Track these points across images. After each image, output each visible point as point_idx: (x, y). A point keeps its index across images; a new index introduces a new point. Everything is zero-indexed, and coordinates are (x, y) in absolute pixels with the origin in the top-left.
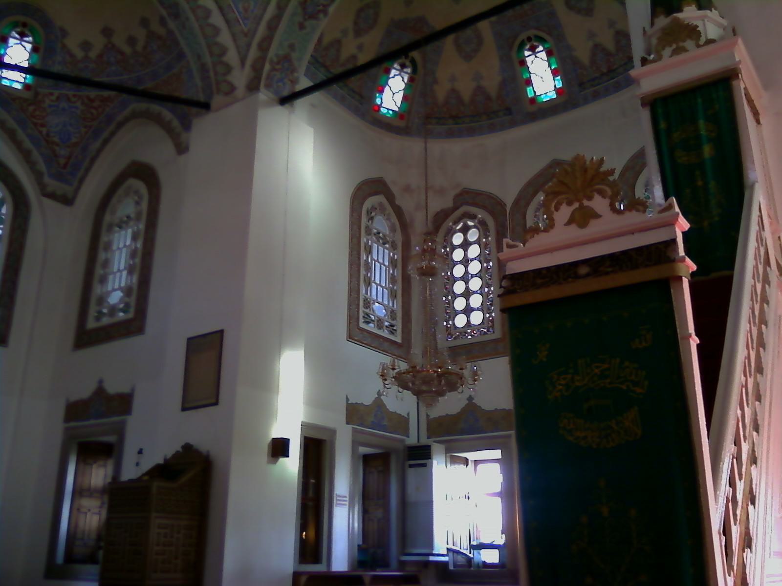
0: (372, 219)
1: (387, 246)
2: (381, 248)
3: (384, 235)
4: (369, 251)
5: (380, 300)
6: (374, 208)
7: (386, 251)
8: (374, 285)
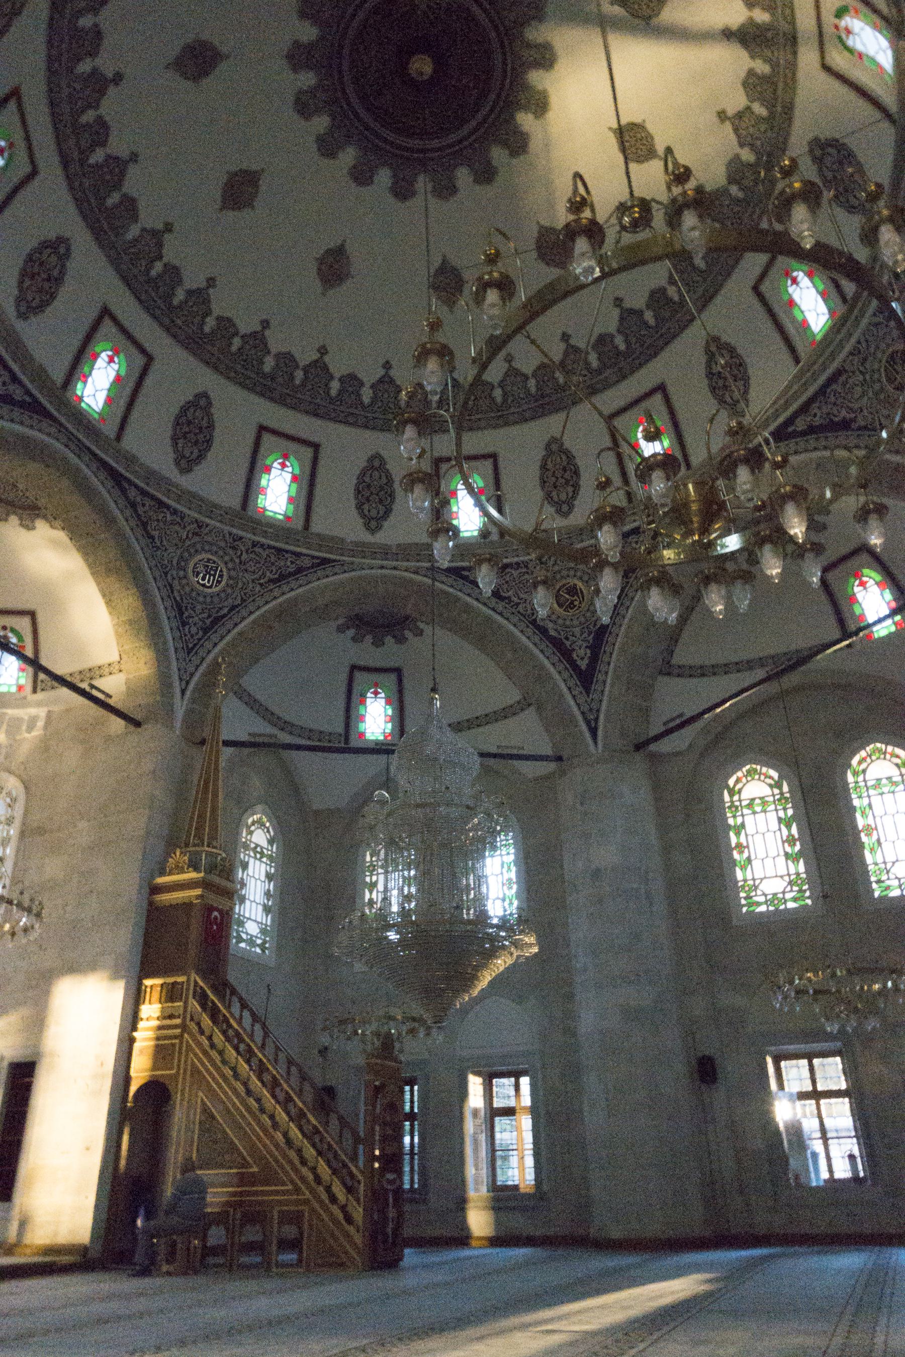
0: (251, 833)
1: (264, 860)
2: (258, 862)
3: (262, 848)
4: (245, 866)
5: (253, 917)
6: (253, 823)
7: (263, 865)
8: (247, 902)
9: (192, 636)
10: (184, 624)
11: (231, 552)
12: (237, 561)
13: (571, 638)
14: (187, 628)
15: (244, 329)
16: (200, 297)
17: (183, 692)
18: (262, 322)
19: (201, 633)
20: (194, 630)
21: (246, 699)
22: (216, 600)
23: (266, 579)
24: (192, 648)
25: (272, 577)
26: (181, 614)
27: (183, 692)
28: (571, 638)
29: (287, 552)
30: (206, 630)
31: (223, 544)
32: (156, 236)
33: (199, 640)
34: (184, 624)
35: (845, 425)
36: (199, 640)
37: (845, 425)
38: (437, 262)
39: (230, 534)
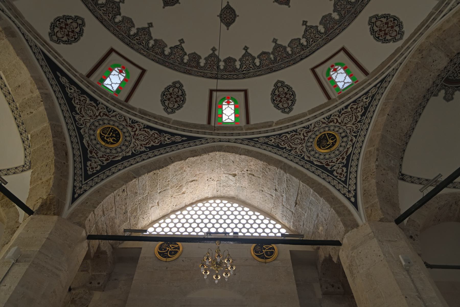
9: (341, 174)
10: (331, 172)
11: (332, 124)
12: (338, 124)
13: (94, 154)
14: (335, 173)
15: (270, 50)
16: (278, 48)
17: (355, 204)
18: (273, 41)
19: (345, 169)
20: (340, 171)
21: (409, 179)
22: (341, 149)
23: (360, 117)
24: (346, 180)
25: (361, 113)
26: (326, 170)
27: (355, 204)
28: (94, 154)
29: (360, 97)
30: (346, 166)
31: (324, 125)
32: (247, 54)
33: (347, 172)
34: (331, 172)
35: (72, 109)
36: (347, 172)
37: (72, 109)
38: (225, 5)
39: (324, 119)
